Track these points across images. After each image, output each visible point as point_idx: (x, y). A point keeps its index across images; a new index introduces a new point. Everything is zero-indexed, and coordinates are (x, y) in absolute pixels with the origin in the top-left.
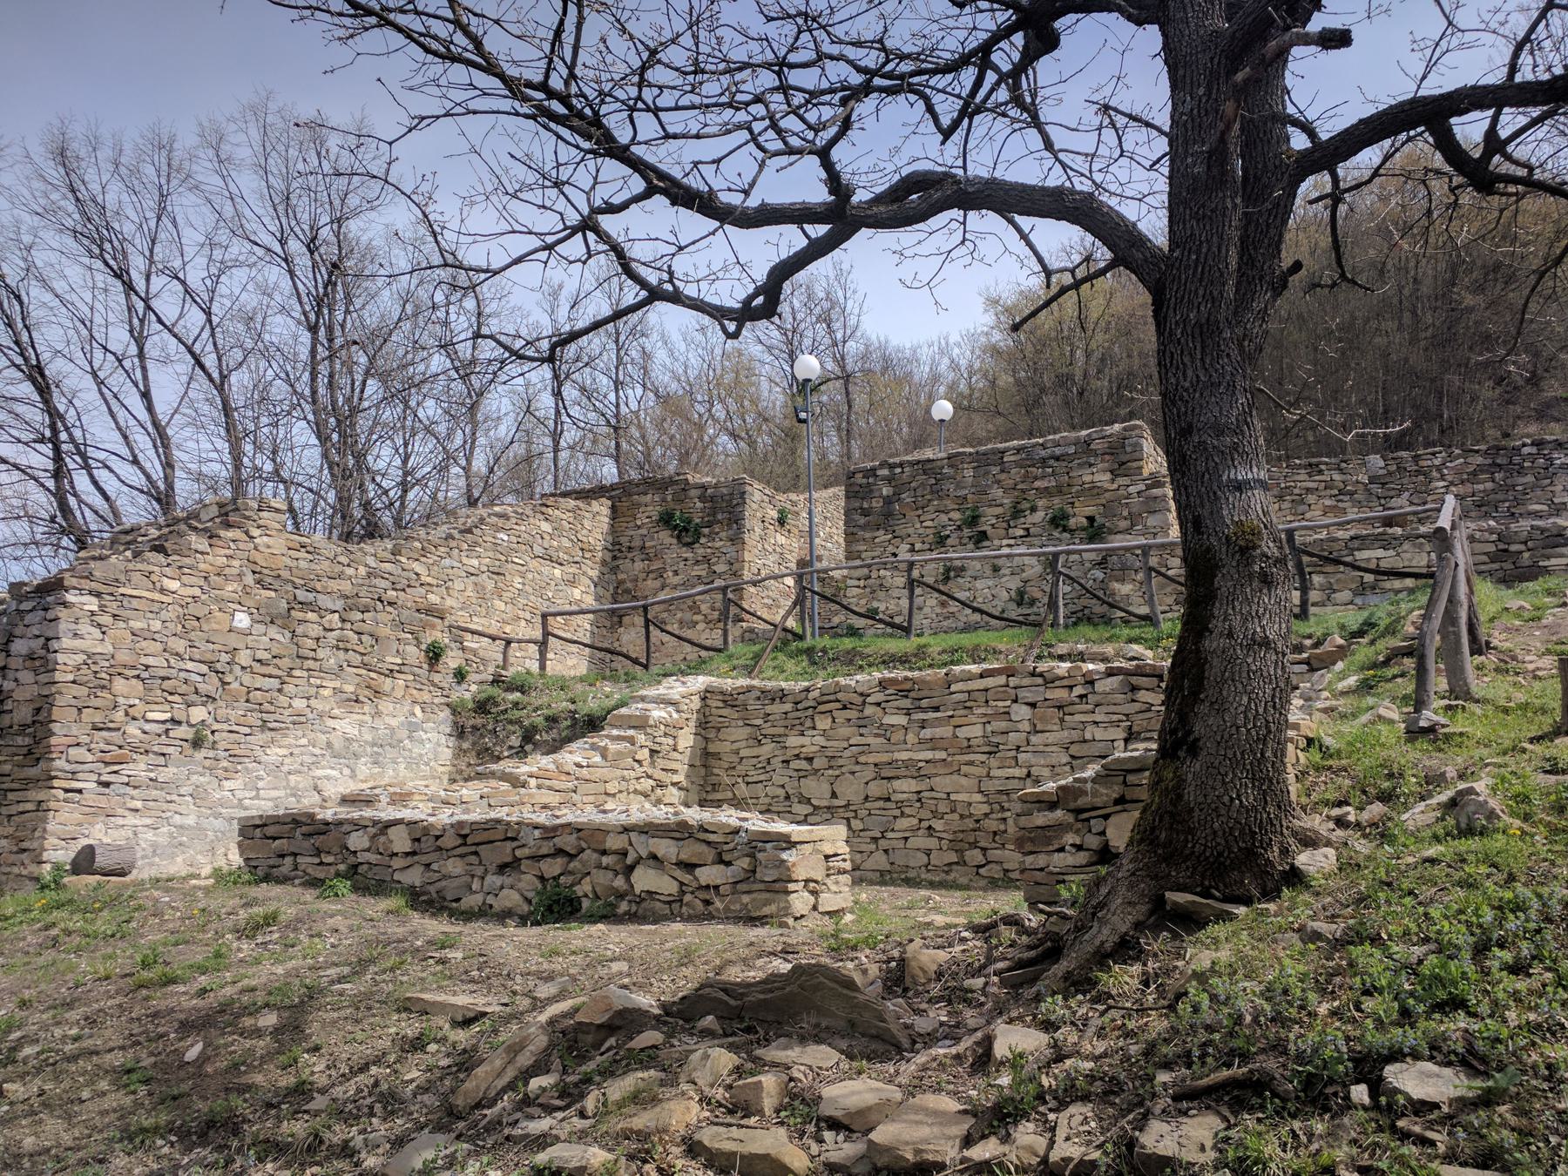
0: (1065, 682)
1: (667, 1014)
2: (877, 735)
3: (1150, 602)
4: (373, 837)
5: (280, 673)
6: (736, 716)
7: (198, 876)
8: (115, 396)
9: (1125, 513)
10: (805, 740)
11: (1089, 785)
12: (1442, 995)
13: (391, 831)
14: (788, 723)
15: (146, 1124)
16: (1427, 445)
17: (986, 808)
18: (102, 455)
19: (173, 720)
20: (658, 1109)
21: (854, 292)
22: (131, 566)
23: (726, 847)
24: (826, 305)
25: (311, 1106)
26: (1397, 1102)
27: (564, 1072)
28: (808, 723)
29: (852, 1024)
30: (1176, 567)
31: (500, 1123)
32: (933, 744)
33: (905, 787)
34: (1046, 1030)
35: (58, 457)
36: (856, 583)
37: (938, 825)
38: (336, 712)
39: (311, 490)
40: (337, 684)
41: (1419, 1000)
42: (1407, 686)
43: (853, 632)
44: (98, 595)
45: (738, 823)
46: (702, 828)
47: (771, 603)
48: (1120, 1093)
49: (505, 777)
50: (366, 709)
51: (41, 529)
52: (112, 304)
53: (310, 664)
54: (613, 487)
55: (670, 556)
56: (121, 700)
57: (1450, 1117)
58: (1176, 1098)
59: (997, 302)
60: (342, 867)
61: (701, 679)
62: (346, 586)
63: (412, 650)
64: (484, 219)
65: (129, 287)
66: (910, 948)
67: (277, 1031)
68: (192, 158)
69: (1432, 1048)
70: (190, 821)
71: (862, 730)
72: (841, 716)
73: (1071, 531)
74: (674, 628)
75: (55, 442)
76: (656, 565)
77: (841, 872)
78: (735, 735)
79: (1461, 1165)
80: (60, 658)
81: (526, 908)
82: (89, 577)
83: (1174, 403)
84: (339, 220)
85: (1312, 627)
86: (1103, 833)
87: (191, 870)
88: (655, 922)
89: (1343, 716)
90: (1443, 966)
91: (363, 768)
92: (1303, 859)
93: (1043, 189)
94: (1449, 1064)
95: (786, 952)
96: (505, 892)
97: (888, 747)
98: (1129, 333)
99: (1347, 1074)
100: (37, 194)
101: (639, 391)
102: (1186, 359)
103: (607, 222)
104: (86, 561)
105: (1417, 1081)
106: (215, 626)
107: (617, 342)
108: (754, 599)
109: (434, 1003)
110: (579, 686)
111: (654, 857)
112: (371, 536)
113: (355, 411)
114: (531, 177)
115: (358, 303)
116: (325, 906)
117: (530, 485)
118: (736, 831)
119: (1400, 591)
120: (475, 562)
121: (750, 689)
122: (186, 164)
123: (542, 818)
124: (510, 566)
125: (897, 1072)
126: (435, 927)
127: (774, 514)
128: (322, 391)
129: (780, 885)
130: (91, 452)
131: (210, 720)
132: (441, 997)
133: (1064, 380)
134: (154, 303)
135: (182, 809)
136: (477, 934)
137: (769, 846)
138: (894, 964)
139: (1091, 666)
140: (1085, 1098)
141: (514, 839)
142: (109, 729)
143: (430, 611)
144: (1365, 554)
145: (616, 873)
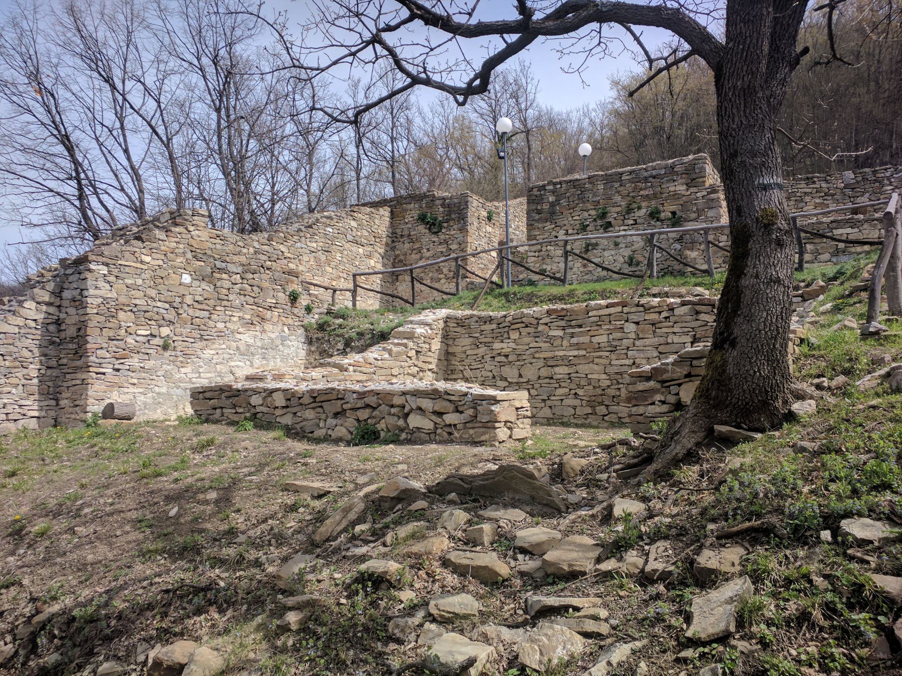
0: (657, 310)
1: (430, 492)
2: (545, 342)
3: (708, 262)
4: (264, 398)
5: (209, 308)
6: (464, 332)
7: (170, 420)
8: (109, 152)
9: (695, 209)
11: (670, 367)
12: (877, 481)
13: (274, 394)
14: (494, 335)
15: (151, 548)
16: (882, 164)
17: (608, 383)
18: (104, 186)
19: (151, 335)
20: (425, 542)
21: (532, 79)
22: (124, 248)
23: (460, 403)
24: (515, 88)
25: (237, 540)
26: (847, 540)
27: (374, 522)
28: (506, 335)
29: (533, 498)
30: (725, 240)
31: (340, 549)
32: (578, 346)
33: (561, 371)
34: (644, 502)
35: (80, 188)
36: (533, 254)
37: (580, 392)
38: (241, 330)
39: (221, 205)
40: (241, 314)
41: (863, 484)
42: (863, 309)
43: (531, 283)
44: (107, 265)
45: (467, 390)
46: (447, 393)
47: (483, 266)
48: (685, 535)
49: (335, 366)
50: (258, 328)
51: (74, 229)
52: (105, 98)
53: (225, 303)
54: (391, 200)
56: (123, 324)
57: (879, 548)
58: (718, 538)
59: (618, 83)
60: (248, 415)
61: (444, 311)
62: (243, 259)
63: (281, 295)
64: (315, 39)
65: (113, 87)
66: (565, 457)
67: (217, 502)
68: (145, 9)
69: (870, 510)
70: (164, 390)
71: (537, 339)
72: (525, 331)
73: (662, 221)
74: (428, 282)
76: (417, 246)
77: (525, 417)
78: (464, 343)
79: (884, 574)
80: (89, 300)
81: (349, 436)
82: (102, 254)
83: (726, 137)
84: (230, 44)
85: (805, 275)
86: (678, 394)
88: (421, 444)
89: (823, 326)
90: (879, 465)
91: (257, 361)
92: (796, 407)
93: (648, 7)
94: (879, 519)
95: (495, 459)
96: (338, 428)
97: (552, 349)
98: (698, 100)
99: (819, 525)
100: (59, 34)
101: (405, 142)
102: (734, 111)
103: (385, 36)
104: (99, 246)
105: (858, 528)
106: (172, 282)
107: (392, 113)
108: (473, 265)
109: (301, 486)
111: (420, 409)
112: (255, 230)
113: (243, 158)
114: (342, 12)
115: (243, 94)
116: (240, 436)
117: (343, 200)
118: (466, 394)
119: (860, 253)
120: (314, 245)
121: (472, 316)
122: (142, 13)
123: (357, 387)
124: (334, 247)
125: (559, 524)
126: (300, 446)
127: (485, 214)
128: (225, 146)
129: (491, 424)
130: (98, 185)
131: (172, 335)
132: (305, 483)
133: (658, 130)
134: (128, 97)
135: (159, 384)
136: (324, 450)
137: (484, 402)
138: (556, 466)
139: (672, 300)
140: (666, 538)
141: (342, 399)
142: (118, 340)
143: (290, 273)
144: (840, 231)
145: (399, 418)
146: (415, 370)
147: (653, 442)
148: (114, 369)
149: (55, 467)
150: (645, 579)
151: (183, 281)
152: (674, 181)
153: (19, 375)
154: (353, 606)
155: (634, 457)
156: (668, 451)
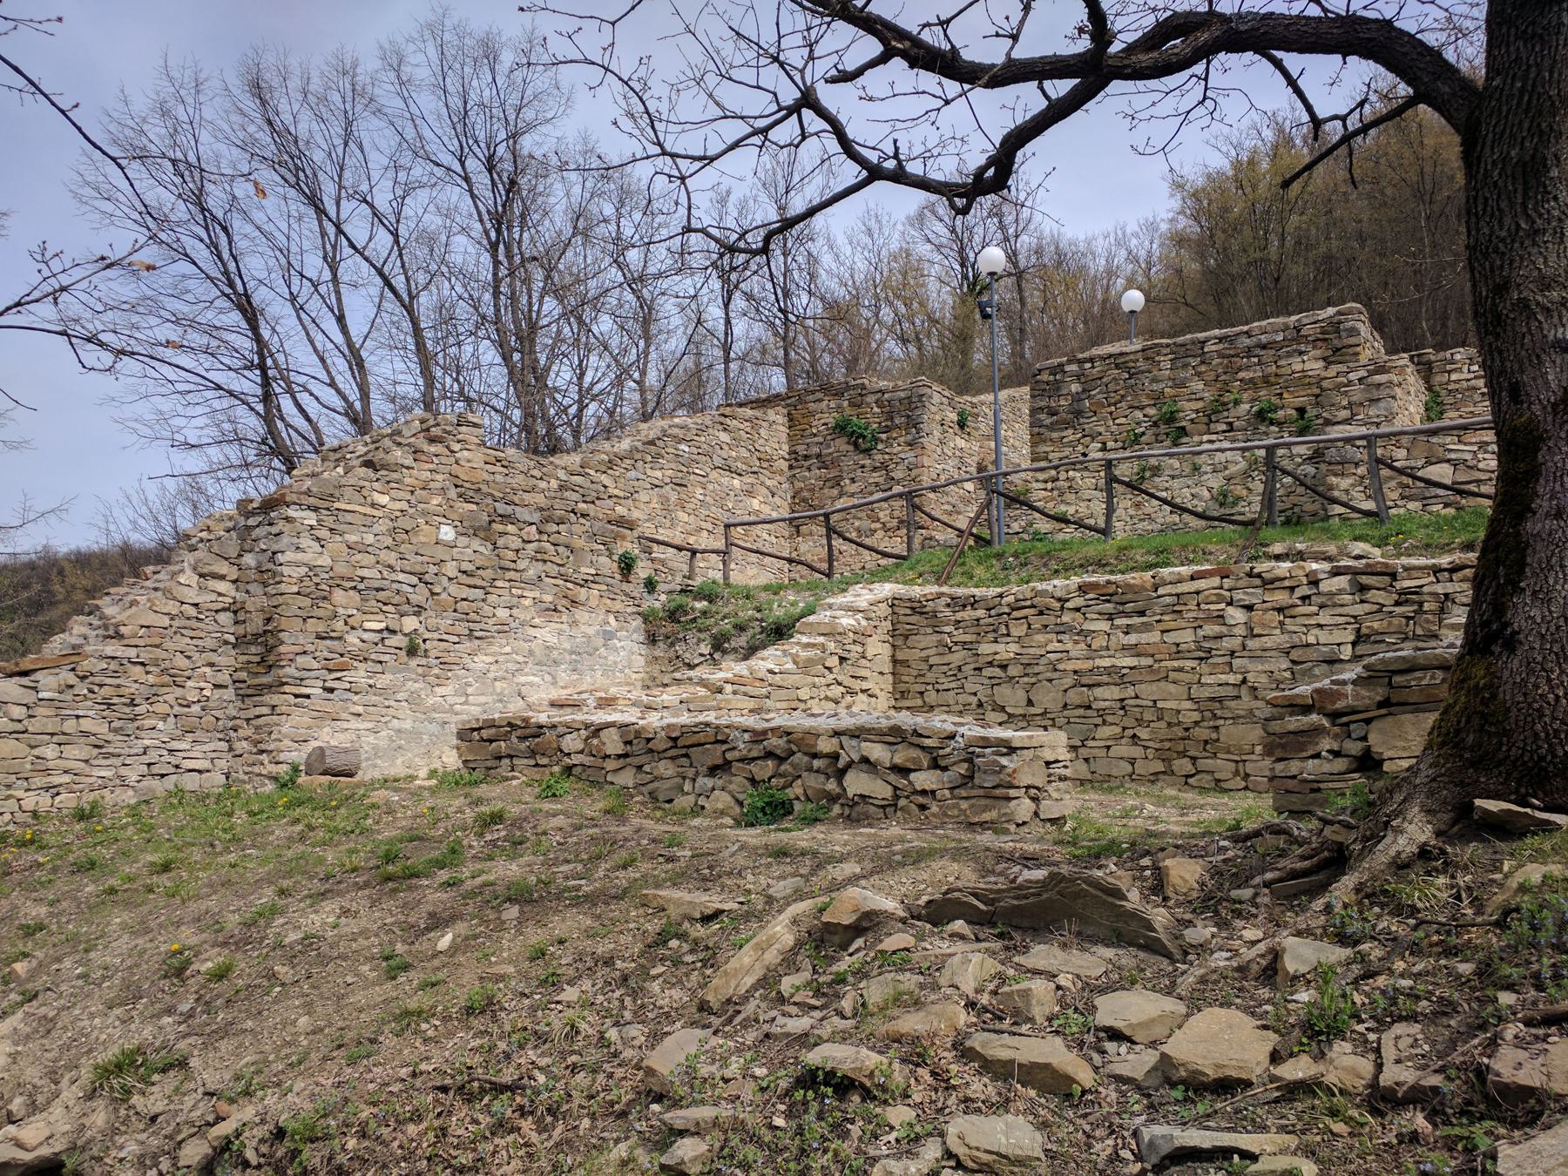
0: (1287, 583)
3: (1378, 495)
10: (1000, 648)
13: (602, 734)
17: (1196, 716)
18: (302, 379)
19: (387, 629)
23: (941, 752)
27: (815, 972)
31: (757, 1021)
35: (266, 382)
37: (1143, 734)
38: (537, 621)
40: (537, 594)
44: (316, 509)
46: (916, 733)
50: (564, 618)
53: (511, 575)
55: (848, 463)
56: (341, 611)
61: (888, 586)
62: (540, 499)
63: (604, 560)
65: (321, 211)
70: (407, 725)
72: (1037, 623)
73: (1279, 424)
74: (853, 535)
75: (263, 368)
80: (286, 570)
83: (1486, 255)
86: (1364, 738)
87: (410, 772)
106: (423, 539)
110: (763, 594)
111: (865, 760)
118: (952, 737)
120: (659, 474)
121: (940, 595)
122: (369, 88)
123: (751, 721)
130: (293, 377)
134: (346, 228)
135: (400, 714)
137: (988, 751)
139: (1314, 566)
140: (1412, 1017)
146: (837, 691)
147: (1343, 830)
148: (325, 689)
149: (232, 858)
150: (1382, 1100)
151: (441, 536)
152: (1301, 353)
153: (170, 698)
154: (800, 1132)
155: (1303, 858)
156: (1380, 847)
